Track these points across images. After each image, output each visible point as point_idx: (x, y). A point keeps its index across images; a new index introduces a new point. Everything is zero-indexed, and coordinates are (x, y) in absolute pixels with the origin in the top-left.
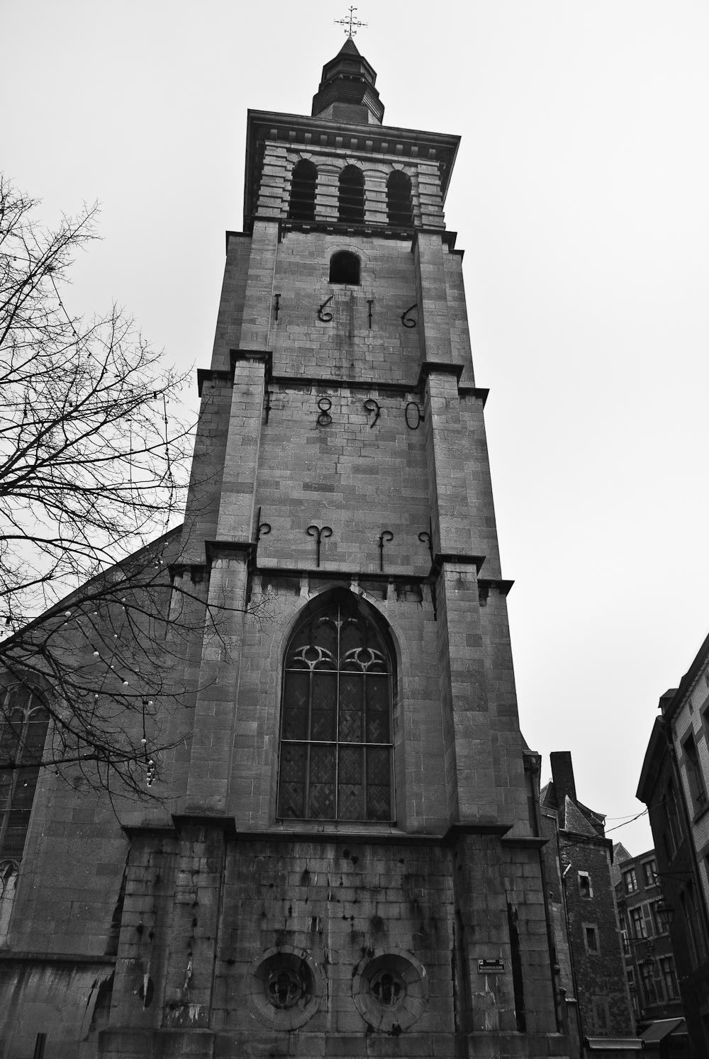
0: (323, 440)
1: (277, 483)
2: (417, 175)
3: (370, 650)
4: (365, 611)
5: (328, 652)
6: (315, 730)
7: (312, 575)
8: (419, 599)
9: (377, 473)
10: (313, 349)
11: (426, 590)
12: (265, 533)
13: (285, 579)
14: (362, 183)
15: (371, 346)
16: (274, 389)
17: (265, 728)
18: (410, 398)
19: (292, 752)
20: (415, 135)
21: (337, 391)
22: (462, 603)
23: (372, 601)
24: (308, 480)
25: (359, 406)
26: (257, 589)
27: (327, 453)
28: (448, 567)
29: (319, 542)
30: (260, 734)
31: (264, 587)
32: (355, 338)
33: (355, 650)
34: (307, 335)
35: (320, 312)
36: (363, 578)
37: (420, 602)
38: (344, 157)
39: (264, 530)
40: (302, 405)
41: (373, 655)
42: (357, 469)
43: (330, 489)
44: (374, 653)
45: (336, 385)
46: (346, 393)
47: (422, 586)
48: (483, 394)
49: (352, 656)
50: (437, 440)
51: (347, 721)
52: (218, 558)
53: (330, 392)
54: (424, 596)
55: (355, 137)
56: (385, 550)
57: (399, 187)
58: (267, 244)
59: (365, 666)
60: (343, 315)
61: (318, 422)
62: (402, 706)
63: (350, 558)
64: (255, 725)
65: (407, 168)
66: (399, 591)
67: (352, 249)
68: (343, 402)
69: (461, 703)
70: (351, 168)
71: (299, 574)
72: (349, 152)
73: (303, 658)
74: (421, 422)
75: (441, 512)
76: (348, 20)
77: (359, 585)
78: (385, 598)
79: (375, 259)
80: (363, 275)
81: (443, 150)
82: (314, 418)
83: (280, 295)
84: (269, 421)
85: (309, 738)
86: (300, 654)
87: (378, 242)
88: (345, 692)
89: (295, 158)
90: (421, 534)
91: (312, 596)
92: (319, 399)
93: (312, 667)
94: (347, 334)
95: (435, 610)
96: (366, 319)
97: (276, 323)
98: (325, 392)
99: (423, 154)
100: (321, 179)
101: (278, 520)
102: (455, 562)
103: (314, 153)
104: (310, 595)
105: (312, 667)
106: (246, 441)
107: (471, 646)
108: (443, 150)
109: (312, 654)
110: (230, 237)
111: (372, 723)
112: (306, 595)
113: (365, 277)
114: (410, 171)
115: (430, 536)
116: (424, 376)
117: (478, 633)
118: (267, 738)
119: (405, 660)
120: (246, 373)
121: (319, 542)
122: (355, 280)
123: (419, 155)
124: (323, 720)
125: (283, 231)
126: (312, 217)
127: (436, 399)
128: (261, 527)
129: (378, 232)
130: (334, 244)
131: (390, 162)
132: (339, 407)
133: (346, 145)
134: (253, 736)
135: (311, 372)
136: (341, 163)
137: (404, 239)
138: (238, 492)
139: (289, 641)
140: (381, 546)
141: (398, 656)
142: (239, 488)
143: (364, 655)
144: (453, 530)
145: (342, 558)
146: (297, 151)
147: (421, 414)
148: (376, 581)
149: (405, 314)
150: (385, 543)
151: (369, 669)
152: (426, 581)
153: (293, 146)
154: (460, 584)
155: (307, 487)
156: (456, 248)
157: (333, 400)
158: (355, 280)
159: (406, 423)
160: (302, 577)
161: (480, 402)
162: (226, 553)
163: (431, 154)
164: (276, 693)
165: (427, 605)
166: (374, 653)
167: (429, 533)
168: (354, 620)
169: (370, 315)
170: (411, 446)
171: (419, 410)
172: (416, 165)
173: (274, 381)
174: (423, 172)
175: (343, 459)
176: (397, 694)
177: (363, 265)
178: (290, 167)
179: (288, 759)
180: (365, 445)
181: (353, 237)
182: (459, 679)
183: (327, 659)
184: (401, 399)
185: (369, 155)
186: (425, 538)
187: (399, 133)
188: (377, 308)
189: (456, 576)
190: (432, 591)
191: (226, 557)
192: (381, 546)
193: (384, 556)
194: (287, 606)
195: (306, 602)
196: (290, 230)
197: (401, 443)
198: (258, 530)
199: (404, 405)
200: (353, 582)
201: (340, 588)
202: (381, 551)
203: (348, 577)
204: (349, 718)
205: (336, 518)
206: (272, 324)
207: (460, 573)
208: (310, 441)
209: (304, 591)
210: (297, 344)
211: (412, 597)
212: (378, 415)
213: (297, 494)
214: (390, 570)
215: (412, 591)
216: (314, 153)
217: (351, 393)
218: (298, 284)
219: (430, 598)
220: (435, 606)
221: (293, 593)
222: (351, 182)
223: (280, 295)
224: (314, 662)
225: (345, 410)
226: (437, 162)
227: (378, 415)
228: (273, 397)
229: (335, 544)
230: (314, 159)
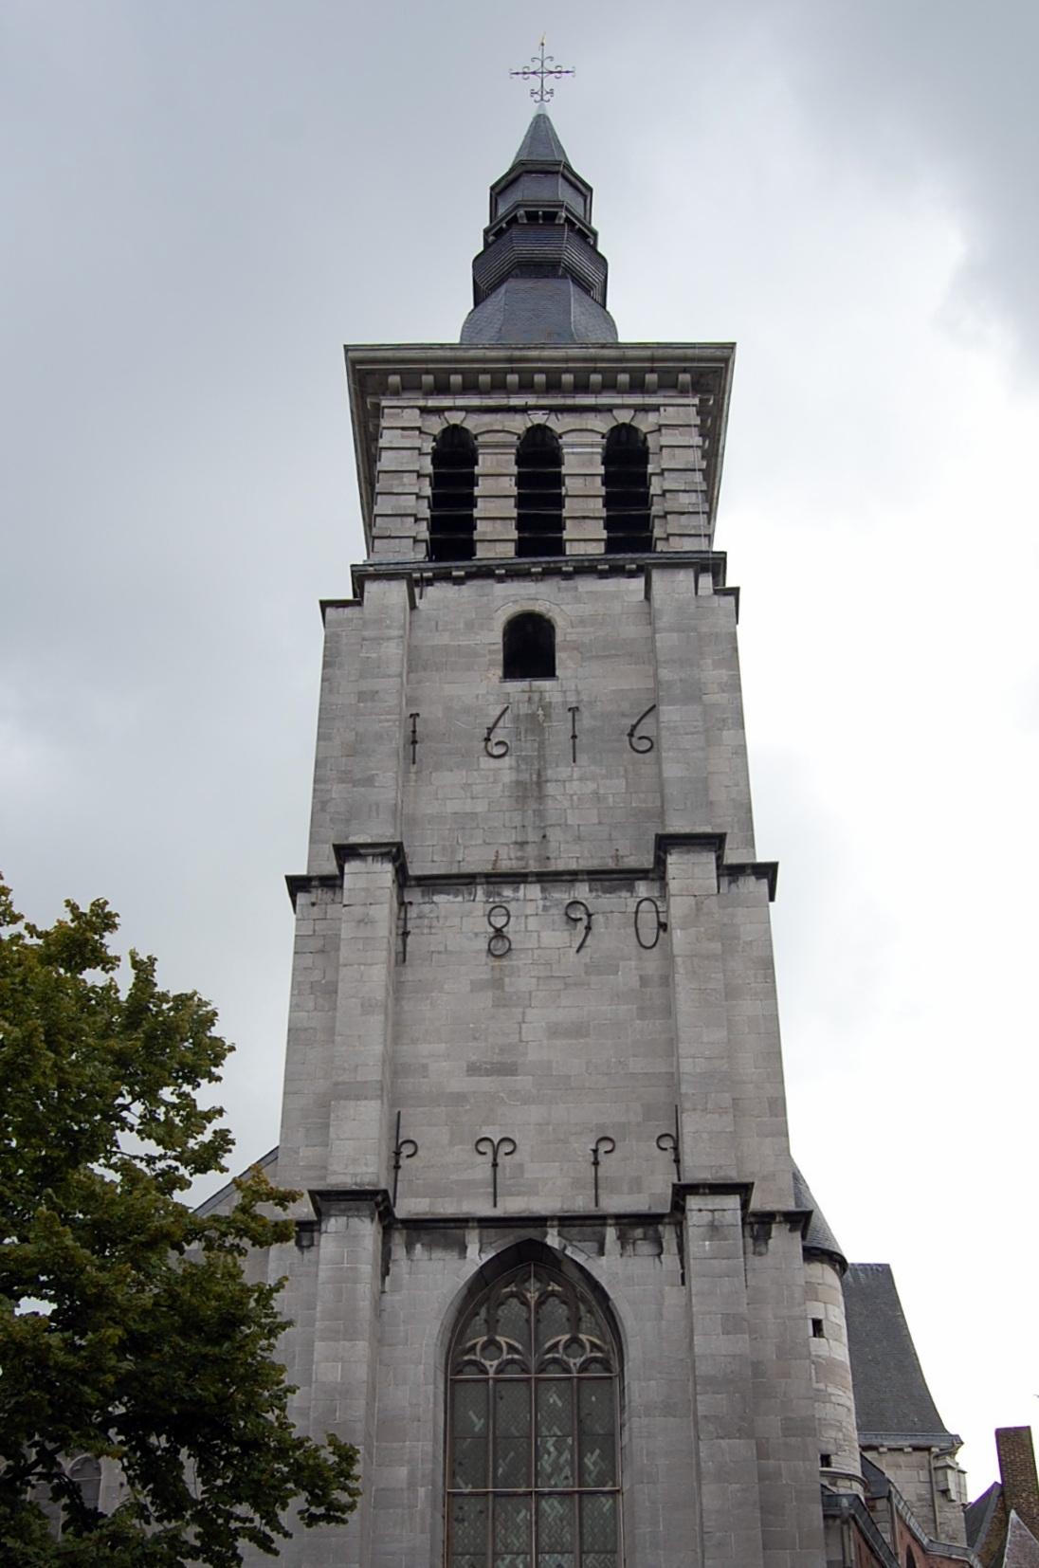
0: (497, 984)
1: (425, 1067)
4: (574, 1274)
7: (485, 1223)
11: (668, 1234)
13: (439, 1231)
14: (558, 461)
16: (414, 895)
20: (648, 353)
21: (516, 890)
23: (580, 1259)
24: (474, 1058)
25: (557, 914)
26: (399, 1252)
28: (693, 1202)
29: (495, 1165)
30: (412, 1485)
31: (409, 1248)
36: (566, 1221)
37: (659, 1255)
38: (524, 410)
39: (407, 1150)
40: (457, 920)
42: (554, 1031)
45: (517, 878)
46: (533, 891)
47: (660, 1228)
49: (554, 1347)
53: (508, 892)
55: (540, 371)
57: (626, 457)
63: (545, 1189)
64: (403, 1472)
65: (640, 416)
66: (623, 1239)
67: (539, 607)
68: (530, 909)
69: (711, 1428)
70: (540, 429)
71: (462, 1222)
72: (532, 401)
75: (687, 1105)
76: (536, 66)
77: (560, 1234)
79: (582, 622)
80: (560, 656)
81: (703, 375)
87: (587, 585)
89: (436, 425)
91: (486, 1257)
97: (413, 769)
98: (499, 894)
99: (668, 383)
100: (484, 464)
101: (427, 1129)
103: (468, 410)
106: (367, 1007)
108: (703, 375)
110: (328, 610)
112: (477, 1256)
114: (645, 423)
115: (673, 1143)
118: (422, 1491)
119: (633, 1352)
120: (361, 883)
121: (495, 1165)
122: (545, 667)
128: (400, 1149)
129: (586, 568)
130: (511, 598)
133: (526, 387)
135: (476, 860)
136: (519, 424)
137: (632, 574)
138: (358, 1098)
140: (596, 1163)
144: (705, 1136)
145: (532, 1191)
146: (439, 411)
149: (634, 727)
150: (601, 1157)
154: (714, 1229)
155: (473, 1070)
157: (512, 907)
158: (545, 667)
170: (644, 981)
172: (656, 408)
177: (559, 638)
178: (429, 446)
185: (569, 401)
188: (586, 721)
189: (706, 1217)
191: (343, 1213)
192: (596, 1163)
194: (440, 1278)
197: (627, 977)
198: (398, 1154)
201: (530, 1241)
203: (540, 1221)
205: (522, 1121)
206: (407, 772)
208: (477, 987)
209: (473, 1250)
210: (452, 807)
211: (646, 1248)
213: (459, 1083)
214: (615, 1203)
215: (644, 1239)
216: (468, 410)
217: (543, 890)
219: (675, 1250)
221: (455, 1254)
222: (539, 457)
224: (495, 1363)
225: (533, 924)
227: (588, 928)
228: (413, 912)
229: (521, 1166)
230: (472, 423)
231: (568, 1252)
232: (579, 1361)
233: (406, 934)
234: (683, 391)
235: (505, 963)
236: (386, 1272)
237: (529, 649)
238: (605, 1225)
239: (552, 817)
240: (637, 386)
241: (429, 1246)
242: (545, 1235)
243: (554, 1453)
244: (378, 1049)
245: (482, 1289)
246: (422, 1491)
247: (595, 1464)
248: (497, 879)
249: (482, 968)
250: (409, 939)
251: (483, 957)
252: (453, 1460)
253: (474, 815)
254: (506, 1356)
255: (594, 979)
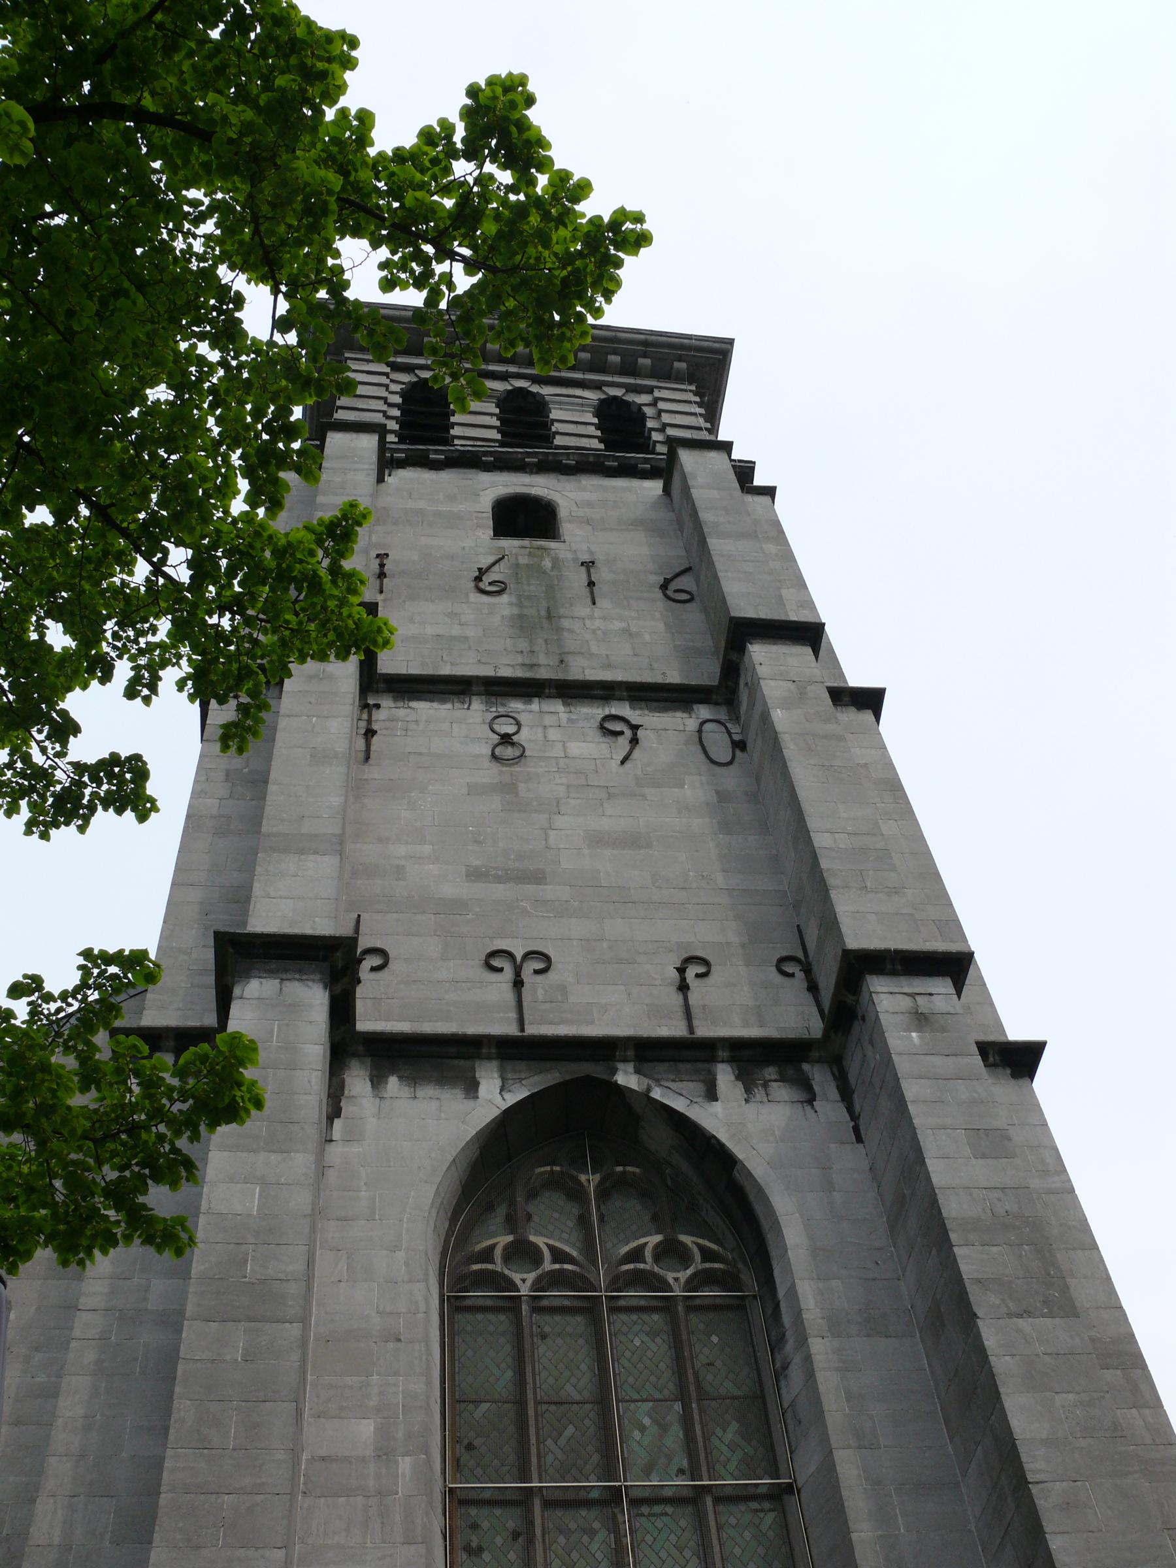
1: (400, 871)
2: (654, 404)
3: (686, 1239)
5: (567, 1249)
6: (550, 1458)
8: (803, 1096)
9: (649, 846)
10: (466, 638)
12: (373, 969)
15: (599, 632)
17: (400, 1435)
18: (704, 712)
19: (485, 1525)
20: (642, 337)
22: (937, 1060)
23: (678, 1104)
24: (477, 863)
27: (519, 811)
29: (518, 984)
30: (385, 1453)
31: (377, 1081)
32: (563, 620)
33: (642, 1241)
34: (451, 615)
35: (478, 579)
36: (648, 1052)
37: (811, 1101)
41: (696, 1251)
43: (538, 878)
44: (697, 1245)
47: (806, 1067)
48: (870, 700)
49: (636, 1255)
50: (791, 750)
51: (643, 1429)
52: (247, 975)
54: (816, 1088)
56: (693, 998)
58: (356, 462)
59: (676, 1279)
60: (529, 584)
61: (494, 756)
62: (808, 1359)
64: (366, 1429)
69: (994, 1299)
73: (498, 1266)
74: (738, 753)
78: (712, 1095)
82: (487, 751)
83: (387, 555)
84: (372, 755)
85: (535, 1475)
86: (487, 1255)
88: (628, 1354)
90: (783, 960)
92: (490, 716)
93: (524, 1291)
94: (543, 613)
95: (854, 1117)
96: (586, 591)
99: (664, 374)
102: (894, 973)
104: (507, 1096)
105: (524, 1291)
106: (320, 757)
107: (984, 1156)
109: (523, 1253)
111: (719, 1431)
112: (497, 1093)
113: (567, 528)
116: (734, 656)
117: (996, 1124)
118: (405, 1465)
121: (518, 984)
123: (653, 375)
124: (570, 1430)
125: (386, 463)
126: (447, 441)
127: (772, 683)
131: (597, 386)
132: (540, 730)
134: (363, 1459)
138: (301, 852)
139: (453, 1219)
140: (683, 987)
141: (770, 1238)
142: (303, 846)
143: (671, 1252)
147: (736, 738)
148: (690, 1054)
151: (691, 1284)
152: (815, 1054)
153: (399, 360)
155: (476, 875)
156: (756, 483)
157: (522, 718)
159: (702, 756)
160: (479, 1057)
161: (868, 716)
162: (273, 966)
163: (679, 371)
164: (427, 1341)
165: (830, 1108)
166: (697, 1245)
167: (800, 954)
168: (629, 1169)
169: (591, 584)
171: (729, 733)
172: (649, 390)
173: (382, 686)
174: (669, 408)
175: (560, 821)
176: (782, 1338)
177: (563, 513)
179: (474, 1545)
180: (610, 796)
181: (537, 473)
182: (971, 1237)
183: (567, 1266)
184: (685, 715)
186: (790, 968)
187: (613, 334)
189: (906, 1003)
190: (835, 1078)
192: (683, 987)
193: (694, 1011)
194: (427, 1131)
195: (495, 1113)
196: (401, 464)
199: (692, 724)
200: (620, 1066)
201: (587, 1080)
202: (686, 999)
203: (606, 1049)
204: (647, 1421)
207: (912, 995)
210: (430, 630)
211: (781, 1091)
212: (634, 741)
218: (424, 541)
219: (834, 1094)
220: (850, 1109)
221: (459, 1093)
223: (387, 555)
224: (531, 1277)
226: (690, 384)
227: (634, 741)
229: (563, 989)
231: (656, 1094)
232: (684, 1275)
233: (370, 733)
234: (678, 379)
235: (517, 769)
236: (335, 1112)
237: (524, 519)
238: (713, 1060)
239: (570, 643)
240: (630, 369)
241: (413, 1080)
242: (614, 1071)
243: (654, 1430)
244: (336, 800)
245: (493, 1172)
246: (405, 1465)
247: (732, 1447)
248: (497, 689)
249: (490, 773)
250: (375, 740)
251: (487, 762)
252: (456, 1440)
253: (466, 639)
254: (548, 1265)
255: (649, 791)
